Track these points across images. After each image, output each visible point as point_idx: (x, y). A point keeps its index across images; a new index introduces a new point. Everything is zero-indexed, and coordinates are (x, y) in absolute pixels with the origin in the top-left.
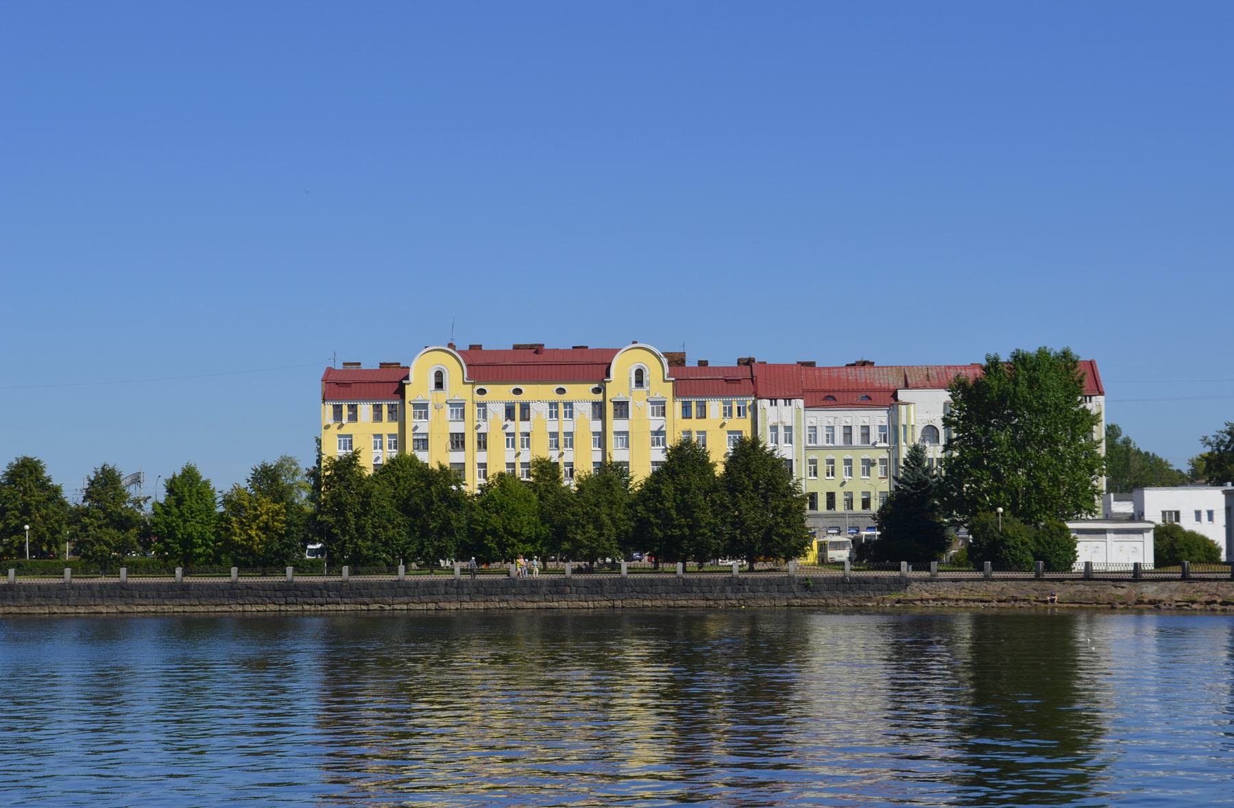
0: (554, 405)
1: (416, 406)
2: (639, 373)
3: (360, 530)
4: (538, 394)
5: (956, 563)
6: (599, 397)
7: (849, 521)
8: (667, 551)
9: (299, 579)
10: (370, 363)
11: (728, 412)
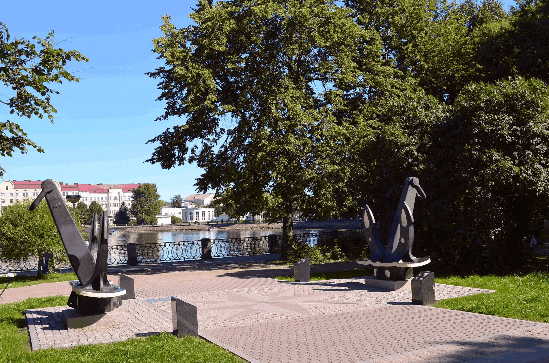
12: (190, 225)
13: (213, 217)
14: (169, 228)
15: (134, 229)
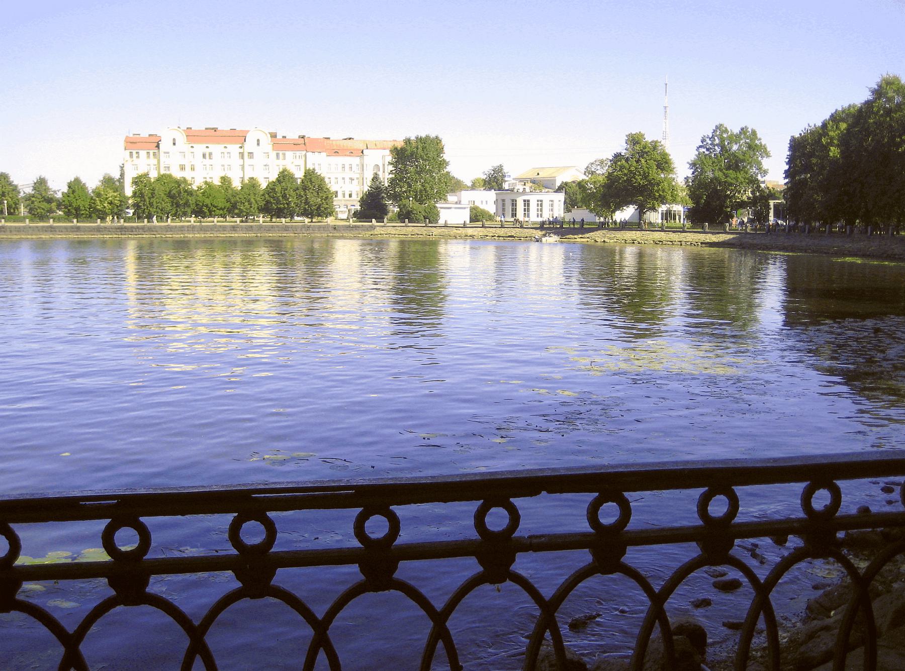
3: (151, 204)
4: (216, 149)
5: (391, 220)
6: (241, 150)
7: (343, 203)
8: (279, 213)
9: (126, 224)
10: (145, 134)
12: (502, 227)
13: (559, 211)
14: (462, 231)
15: (393, 231)
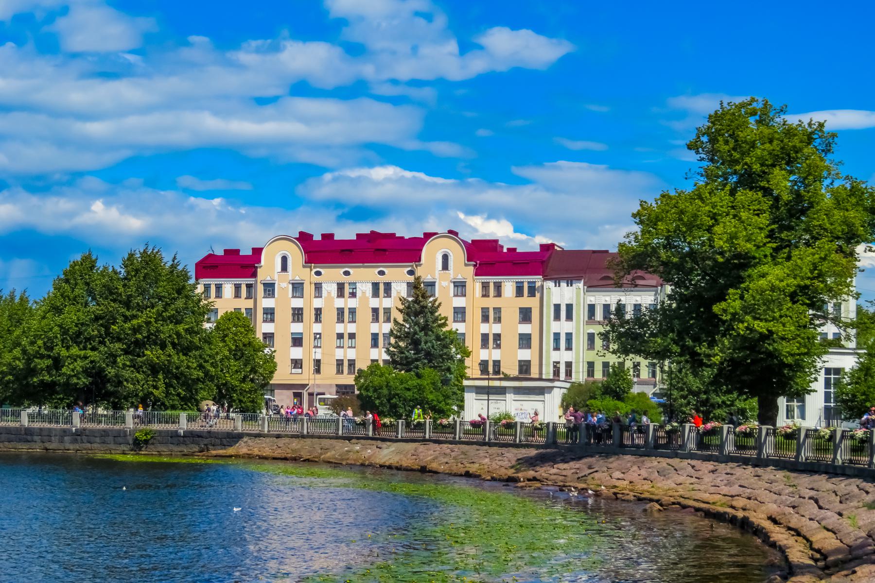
0: (376, 286)
1: (266, 285)
2: (284, 259)
6: (411, 279)
11: (519, 292)
